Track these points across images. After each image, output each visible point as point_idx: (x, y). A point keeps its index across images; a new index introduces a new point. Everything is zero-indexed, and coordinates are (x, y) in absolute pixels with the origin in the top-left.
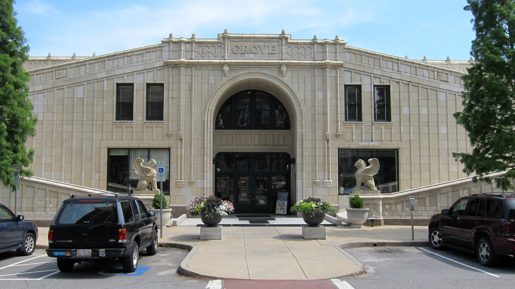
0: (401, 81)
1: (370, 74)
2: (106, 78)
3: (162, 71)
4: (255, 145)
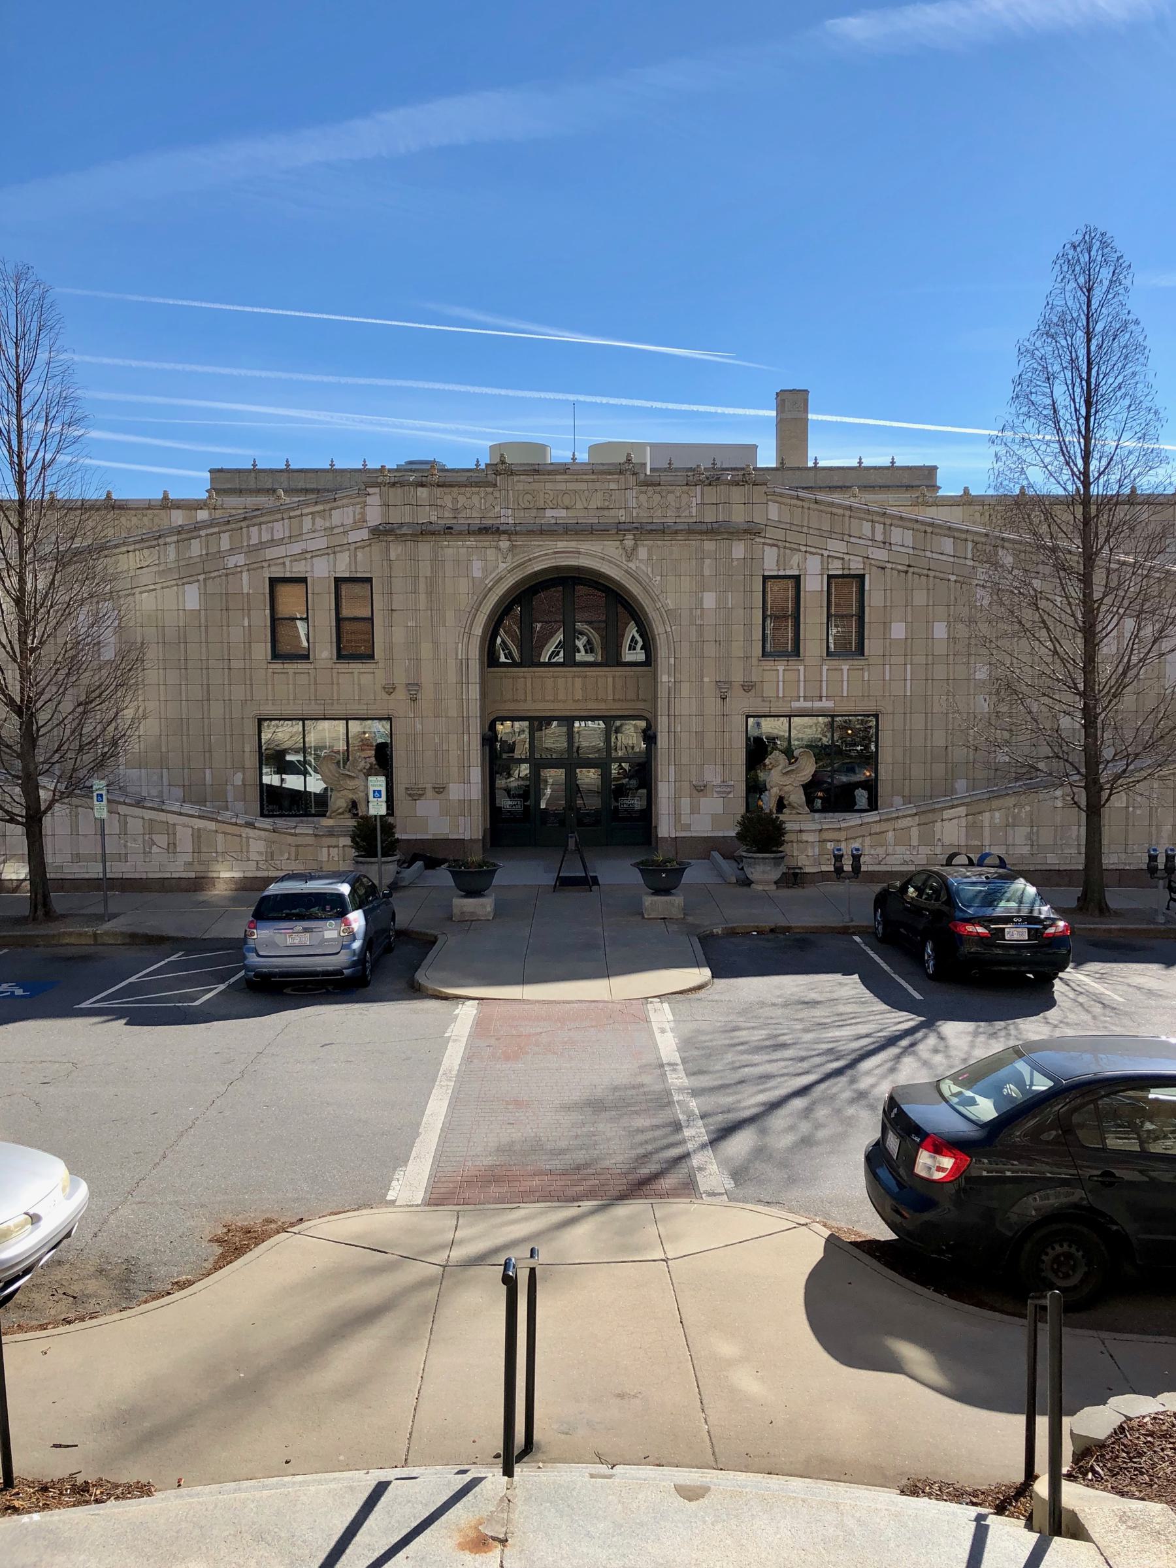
0: (889, 565)
1: (820, 551)
2: (246, 567)
3: (368, 549)
4: (575, 701)
